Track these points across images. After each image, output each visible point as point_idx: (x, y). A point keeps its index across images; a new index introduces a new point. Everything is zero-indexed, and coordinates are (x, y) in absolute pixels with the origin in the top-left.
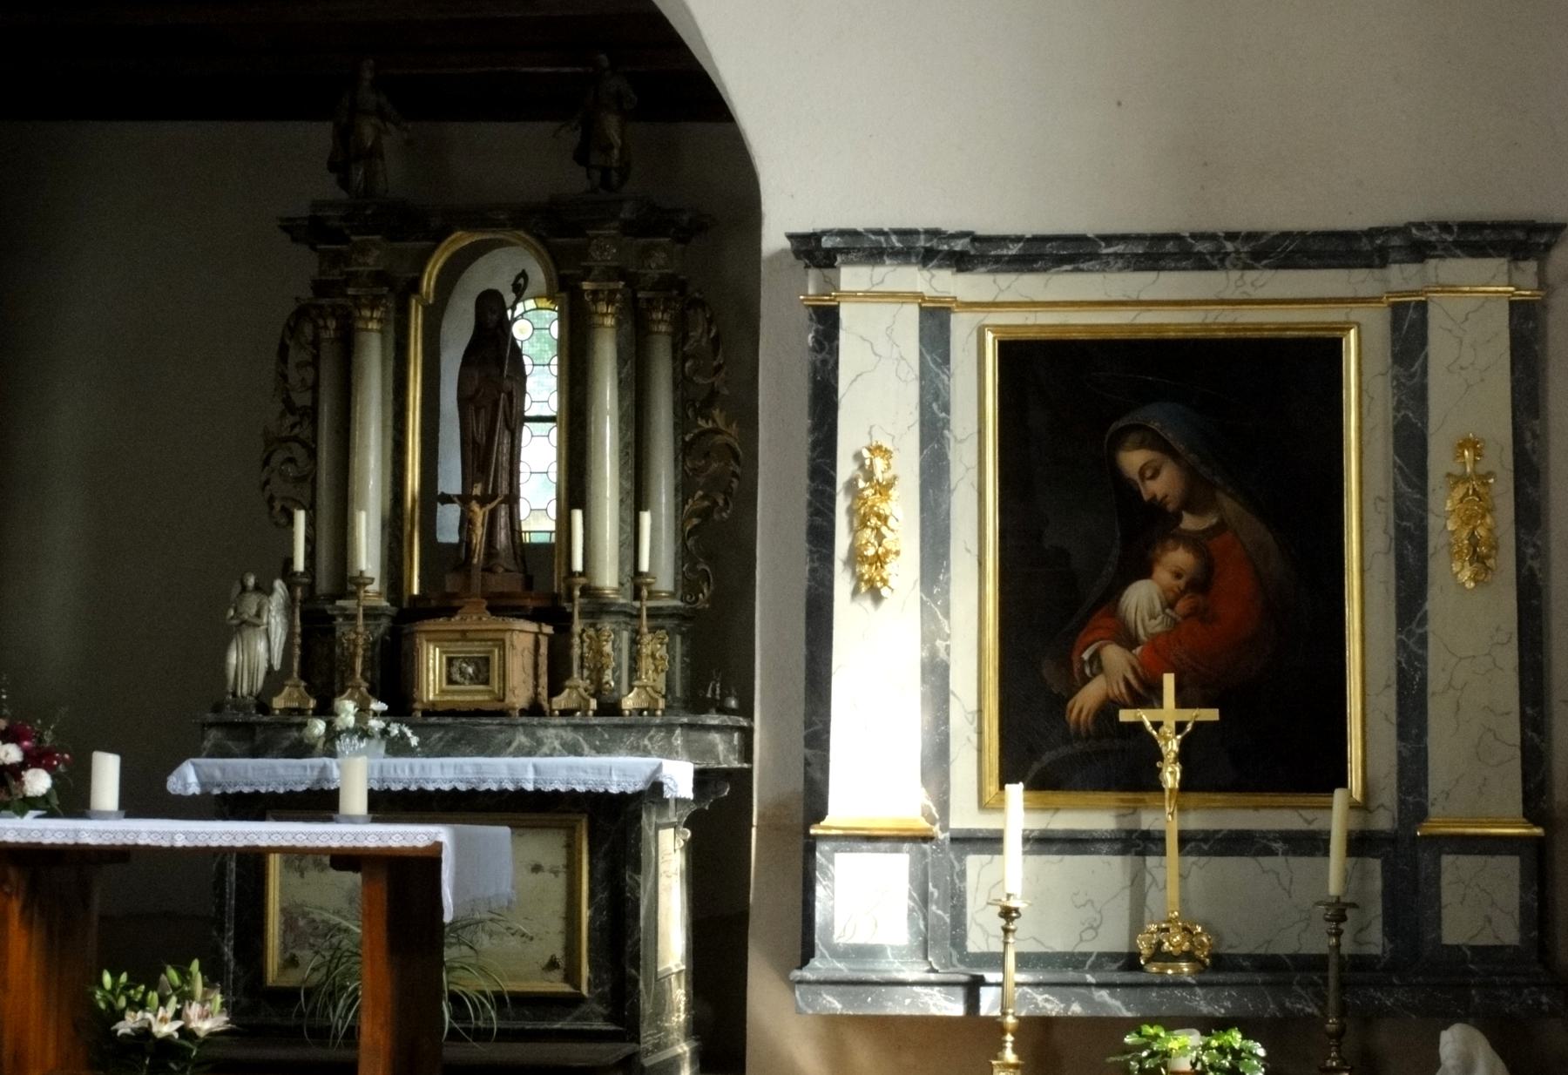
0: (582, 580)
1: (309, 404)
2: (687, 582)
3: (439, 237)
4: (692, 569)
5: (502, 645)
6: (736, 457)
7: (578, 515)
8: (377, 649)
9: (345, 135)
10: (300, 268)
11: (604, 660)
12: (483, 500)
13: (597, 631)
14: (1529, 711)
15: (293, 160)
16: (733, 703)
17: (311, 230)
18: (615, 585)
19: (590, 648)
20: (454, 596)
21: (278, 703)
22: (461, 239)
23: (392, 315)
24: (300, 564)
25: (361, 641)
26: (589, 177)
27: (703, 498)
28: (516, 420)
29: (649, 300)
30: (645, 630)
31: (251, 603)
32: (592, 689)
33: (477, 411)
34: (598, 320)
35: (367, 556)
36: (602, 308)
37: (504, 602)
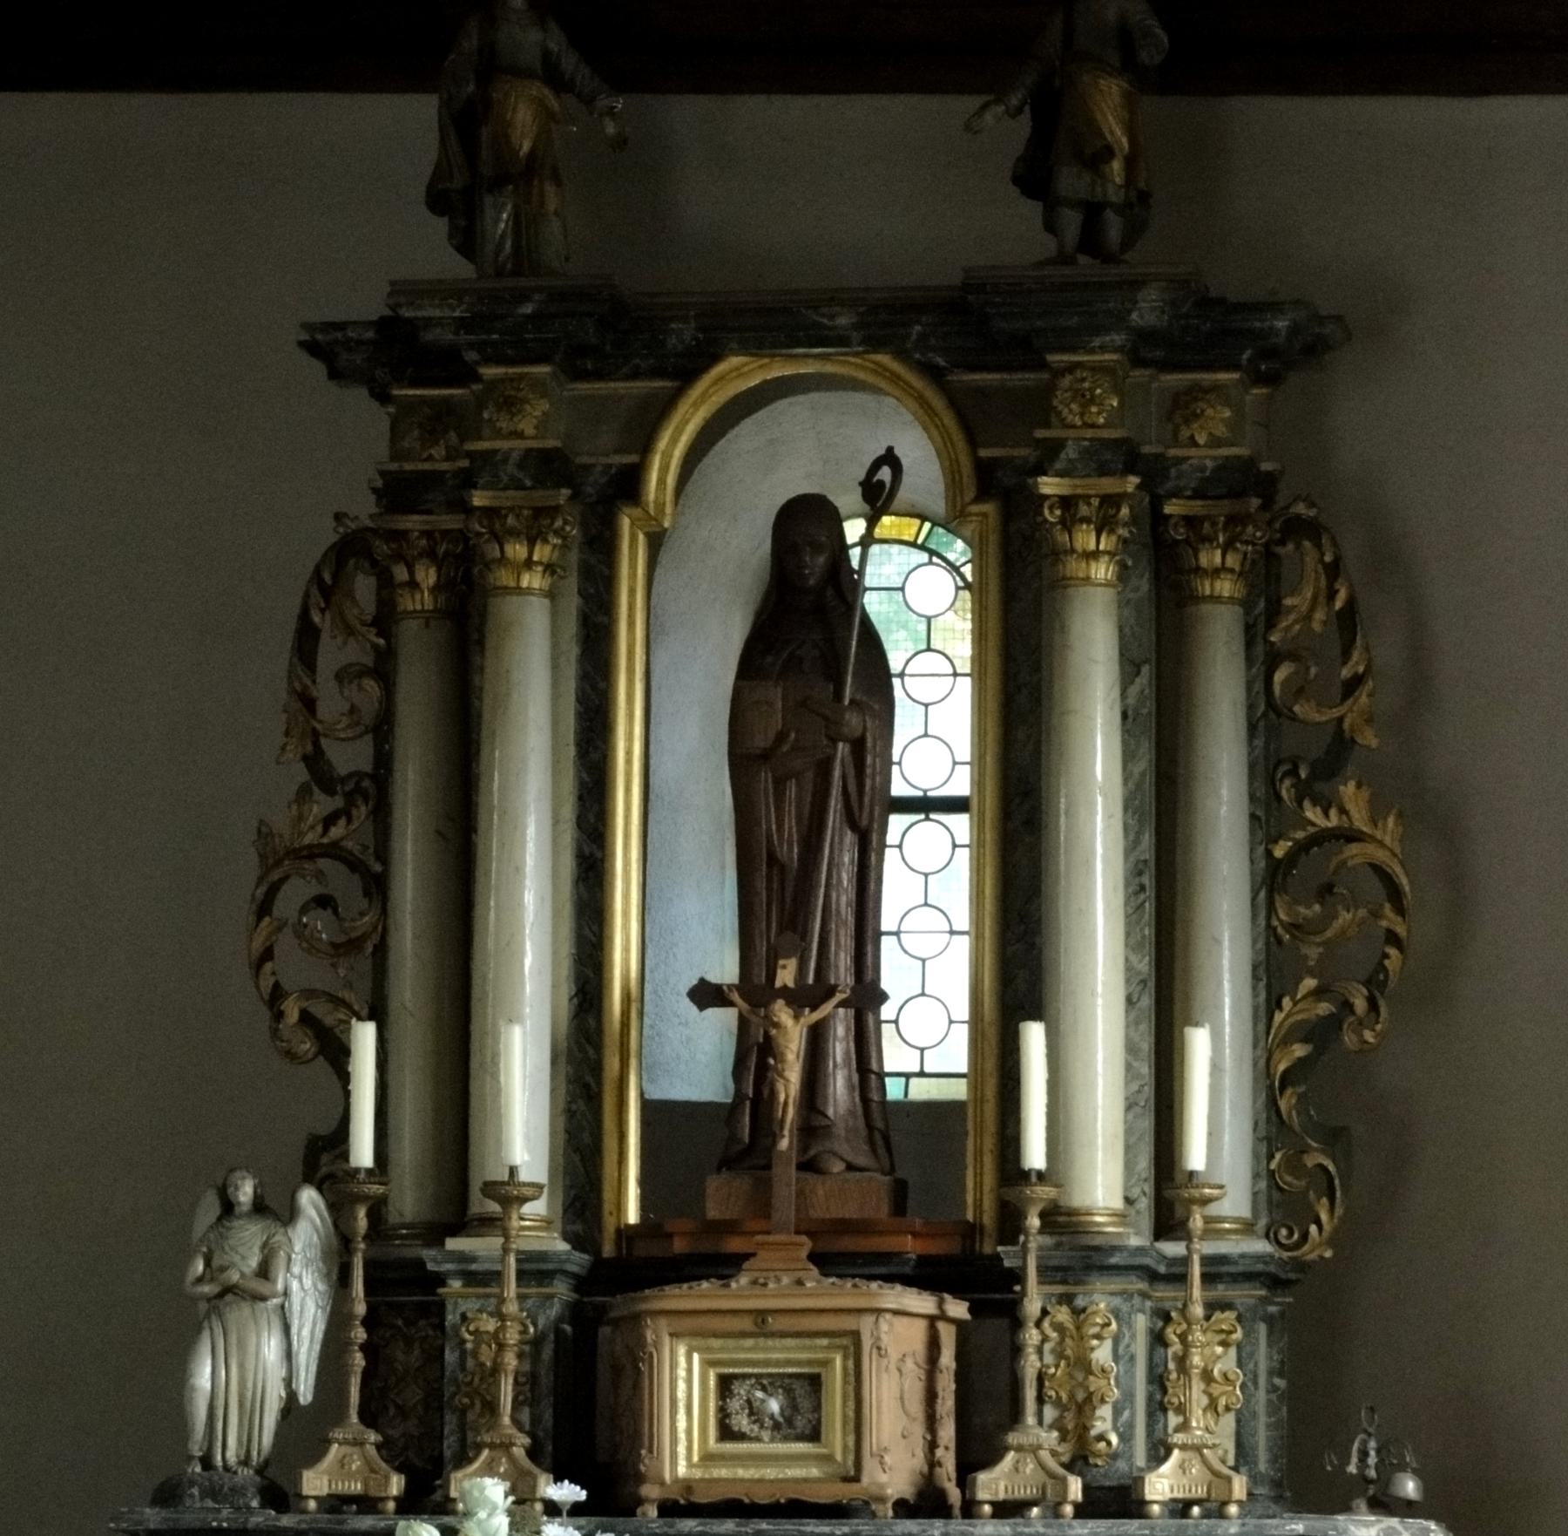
0: (1045, 1192)
1: (368, 767)
2: (1281, 1204)
3: (687, 371)
4: (1294, 1164)
5: (853, 1345)
6: (1394, 894)
7: (1034, 1036)
8: (547, 1352)
9: (467, 124)
10: (345, 445)
11: (1095, 1383)
12: (805, 997)
13: (1077, 1312)
14: (592, 1022)
15: (335, 187)
16: (1410, 1487)
17: (385, 353)
18: (1117, 1203)
19: (1060, 1355)
20: (729, 1227)
21: (315, 1483)
22: (737, 373)
23: (574, 557)
24: (363, 1152)
25: (512, 1336)
26: (1050, 226)
27: (1318, 994)
28: (869, 808)
29: (1190, 521)
30: (1198, 1310)
31: (245, 1245)
32: (1066, 1451)
33: (780, 784)
34: (1074, 567)
35: (522, 1128)
36: (1086, 539)
37: (848, 1244)
